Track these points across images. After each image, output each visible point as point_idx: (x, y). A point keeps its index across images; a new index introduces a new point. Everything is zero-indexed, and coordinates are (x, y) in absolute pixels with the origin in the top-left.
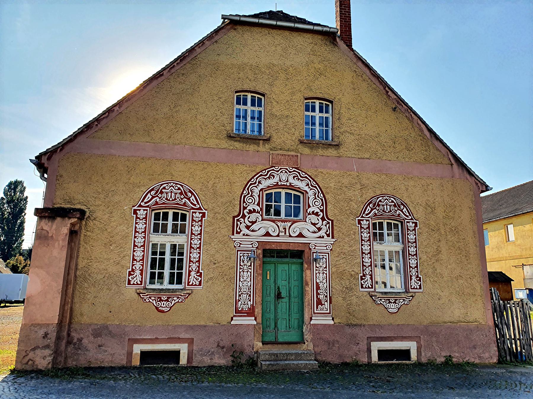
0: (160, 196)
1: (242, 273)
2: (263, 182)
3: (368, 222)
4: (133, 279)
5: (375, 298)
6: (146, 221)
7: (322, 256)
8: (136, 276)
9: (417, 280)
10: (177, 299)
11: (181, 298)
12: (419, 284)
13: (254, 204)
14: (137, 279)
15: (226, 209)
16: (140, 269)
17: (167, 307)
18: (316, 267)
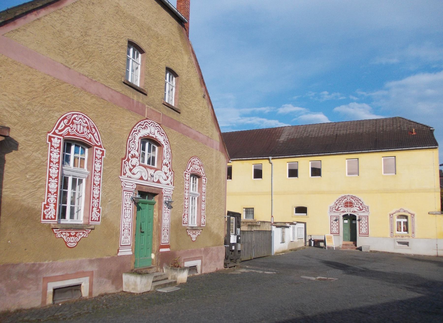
0: (71, 126)
1: (125, 210)
2: (141, 131)
3: (59, 141)
4: (48, 213)
5: (56, 231)
6: (60, 151)
7: (130, 194)
8: (51, 209)
9: (97, 211)
10: (83, 234)
11: (85, 233)
12: (98, 216)
13: (135, 149)
14: (51, 213)
15: (117, 150)
16: (54, 202)
17: (74, 242)
18: (125, 204)
